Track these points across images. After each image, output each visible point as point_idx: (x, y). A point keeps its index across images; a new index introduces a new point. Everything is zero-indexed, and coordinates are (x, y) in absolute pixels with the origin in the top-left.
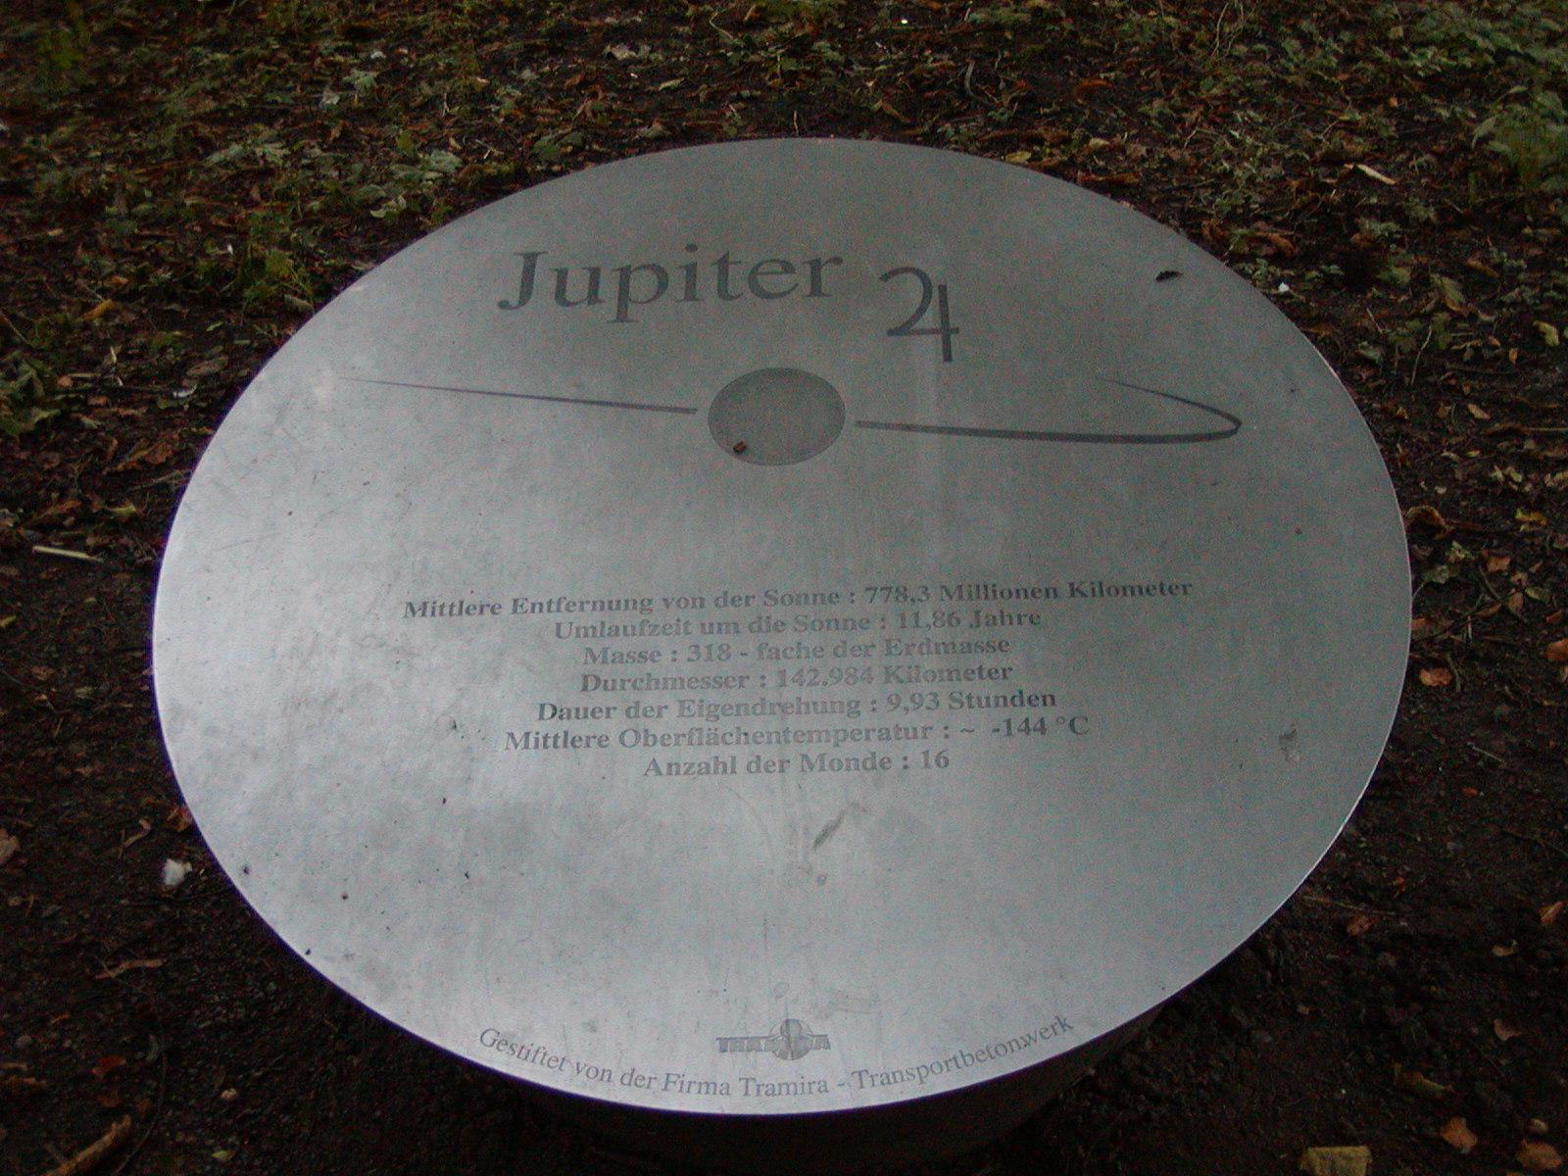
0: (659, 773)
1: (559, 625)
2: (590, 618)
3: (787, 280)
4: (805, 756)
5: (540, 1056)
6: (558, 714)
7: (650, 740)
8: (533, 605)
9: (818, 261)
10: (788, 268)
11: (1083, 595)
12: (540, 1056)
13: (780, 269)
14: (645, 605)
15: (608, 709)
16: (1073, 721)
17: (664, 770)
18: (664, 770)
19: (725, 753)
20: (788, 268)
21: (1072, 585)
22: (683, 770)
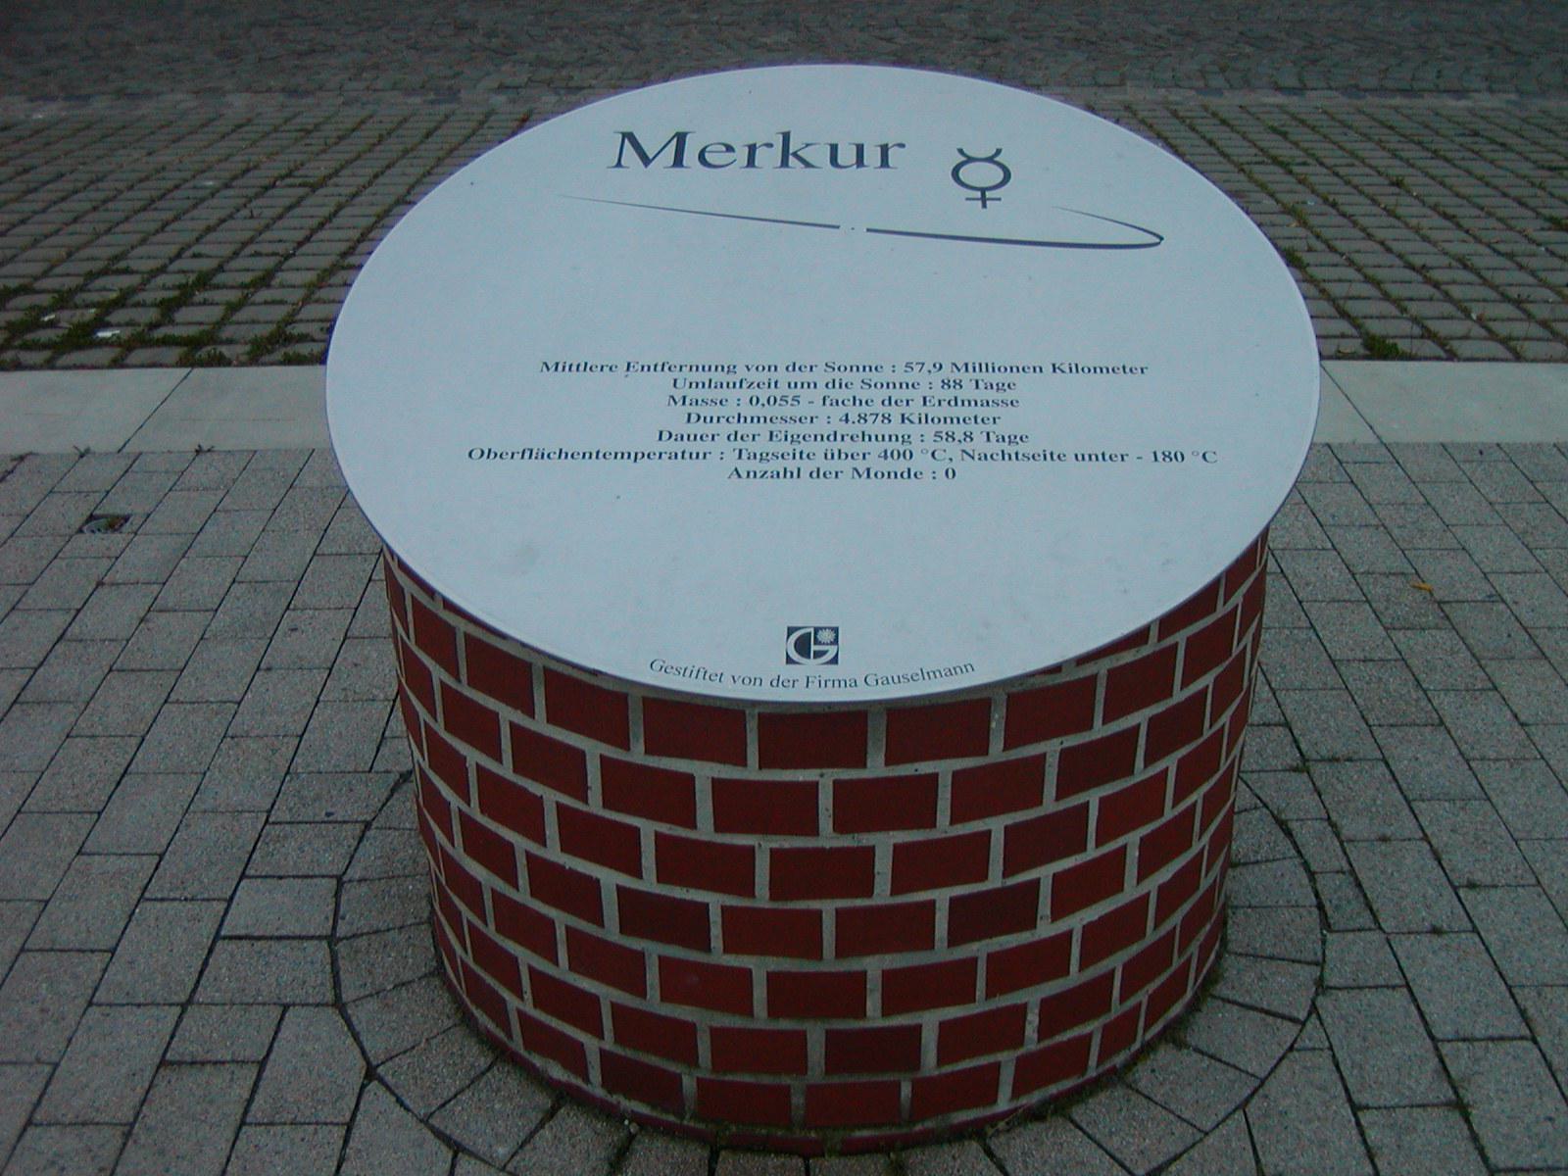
0: (739, 476)
1: (675, 381)
2: (1022, 448)
3: (728, 157)
4: (856, 469)
5: (701, 674)
6: (674, 437)
7: (843, 456)
8: (643, 367)
9: (755, 145)
10: (729, 149)
11: (912, 422)
12: (701, 674)
13: (724, 149)
14: (732, 369)
15: (713, 436)
16: (1204, 455)
17: (744, 475)
18: (744, 475)
19: (791, 466)
20: (729, 149)
21: (1054, 365)
22: (758, 475)
